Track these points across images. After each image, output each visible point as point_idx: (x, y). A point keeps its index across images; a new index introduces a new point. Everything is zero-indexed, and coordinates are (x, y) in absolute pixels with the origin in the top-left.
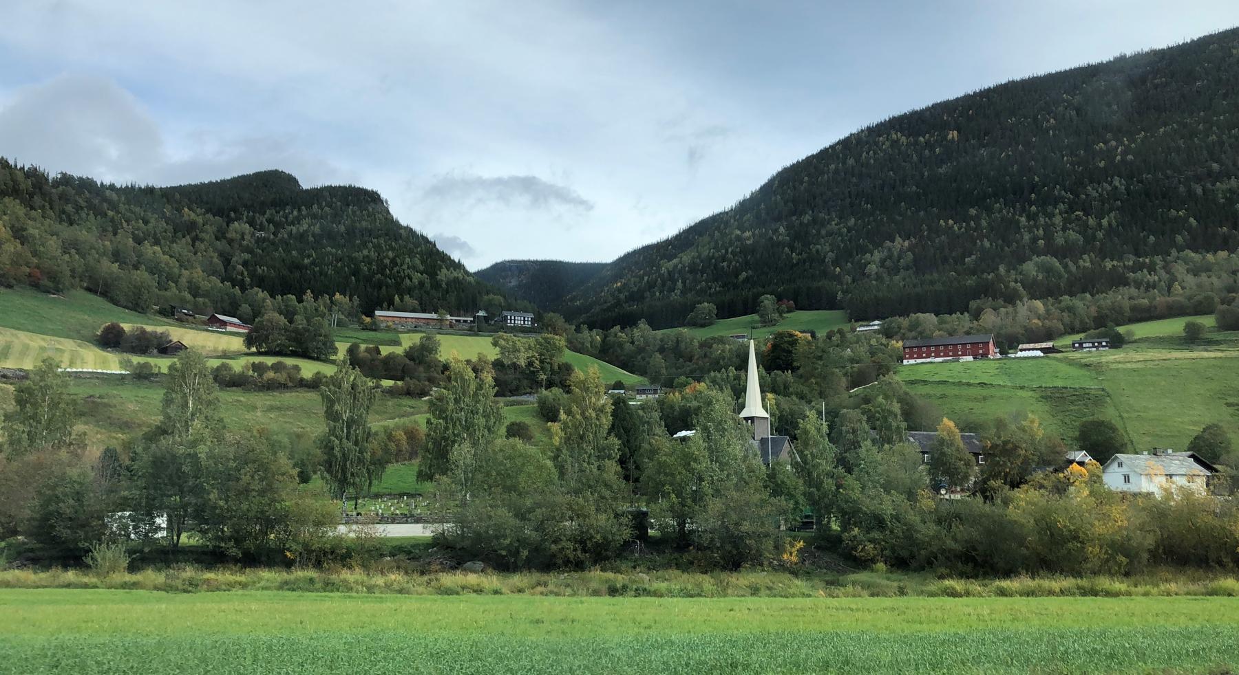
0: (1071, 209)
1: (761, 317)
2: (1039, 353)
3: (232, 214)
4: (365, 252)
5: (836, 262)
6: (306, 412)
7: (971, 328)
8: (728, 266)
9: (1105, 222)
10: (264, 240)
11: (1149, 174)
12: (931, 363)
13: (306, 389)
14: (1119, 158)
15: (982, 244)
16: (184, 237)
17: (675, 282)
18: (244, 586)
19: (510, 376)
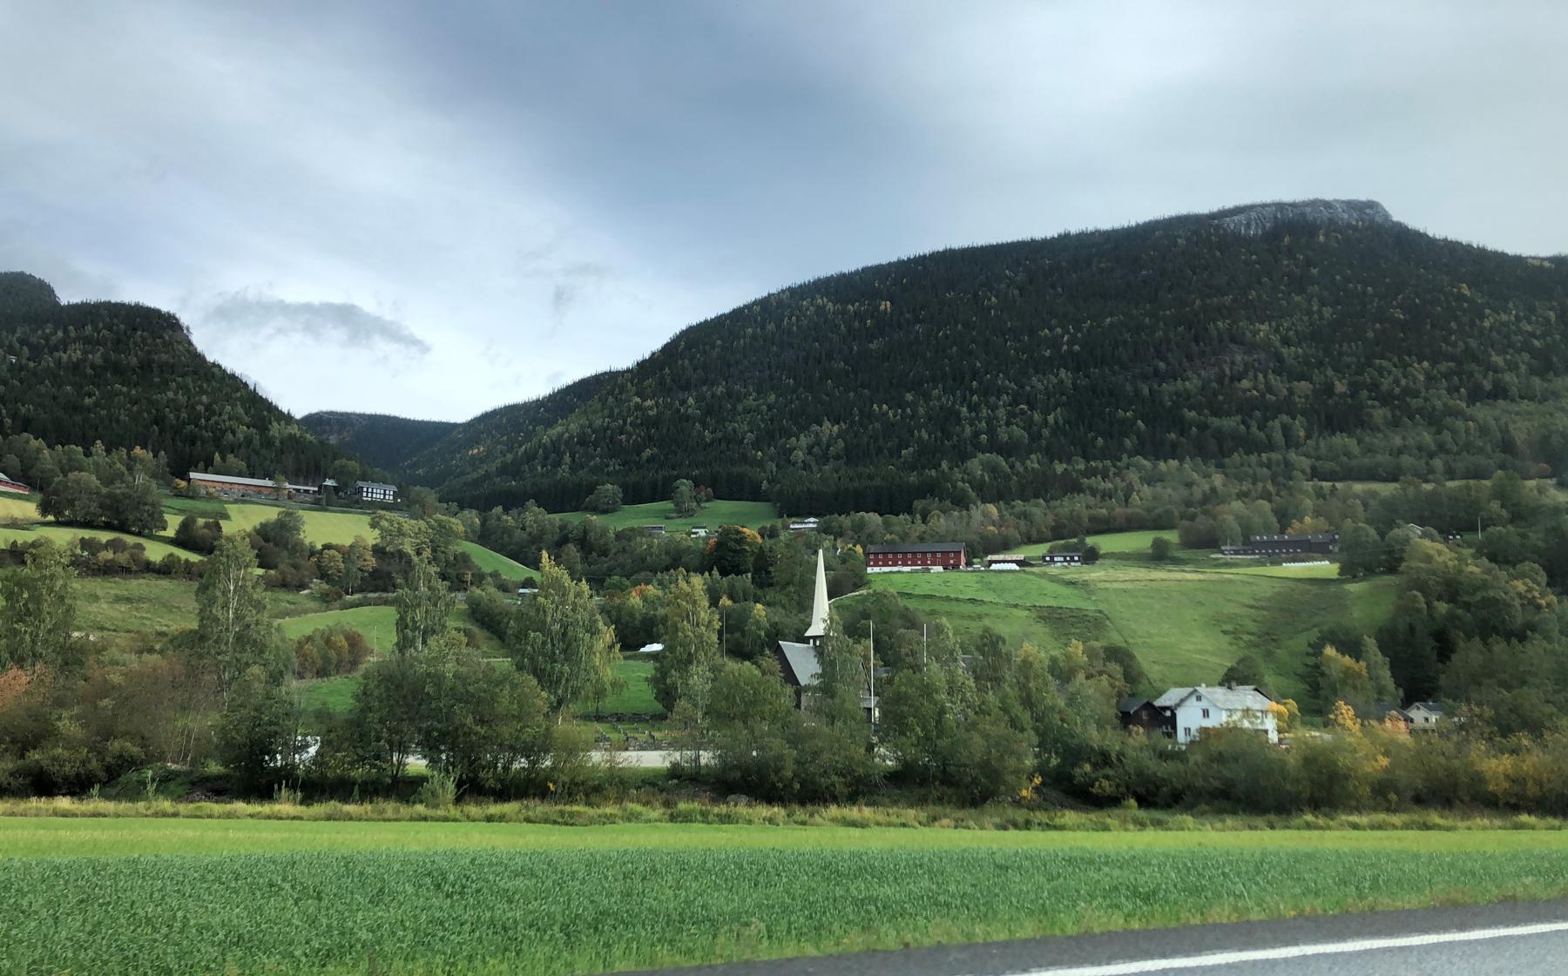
0: (1015, 403)
2: (1014, 567)
4: (170, 394)
5: (757, 445)
6: (164, 605)
7: (924, 532)
9: (1051, 418)
11: (1095, 368)
12: (899, 572)
13: (155, 575)
14: (1065, 347)
17: (560, 455)
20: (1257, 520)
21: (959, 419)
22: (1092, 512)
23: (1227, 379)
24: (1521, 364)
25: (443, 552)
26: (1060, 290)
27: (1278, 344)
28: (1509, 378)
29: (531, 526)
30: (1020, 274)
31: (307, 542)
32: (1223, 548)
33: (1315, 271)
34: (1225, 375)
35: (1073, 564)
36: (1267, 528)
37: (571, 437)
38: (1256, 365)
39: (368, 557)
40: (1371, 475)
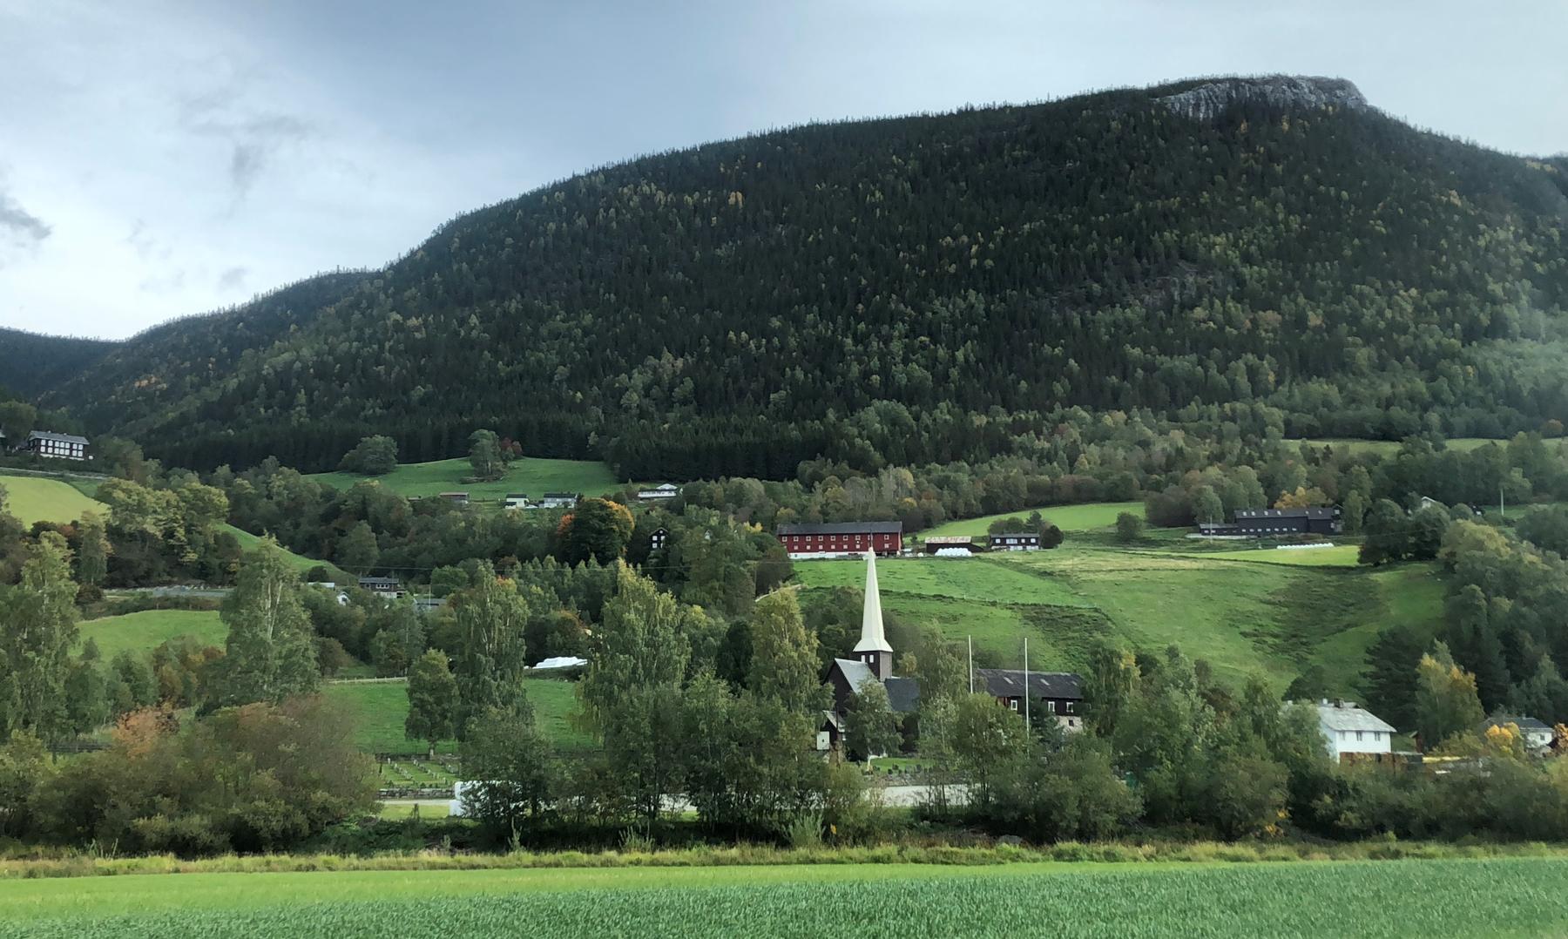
1: (473, 465)
2: (965, 552)
5: (573, 381)
8: (388, 373)
9: (960, 355)
14: (974, 262)
15: (793, 375)
17: (291, 394)
19: (134, 554)
20: (1242, 491)
21: (843, 355)
22: (1030, 478)
23: (1176, 306)
24: (1522, 294)
26: (963, 184)
27: (1237, 261)
28: (1509, 311)
30: (912, 162)
32: (1202, 526)
33: (1279, 168)
34: (1174, 302)
35: (1028, 548)
36: (1253, 501)
37: (305, 368)
38: (1212, 289)
40: (1359, 434)
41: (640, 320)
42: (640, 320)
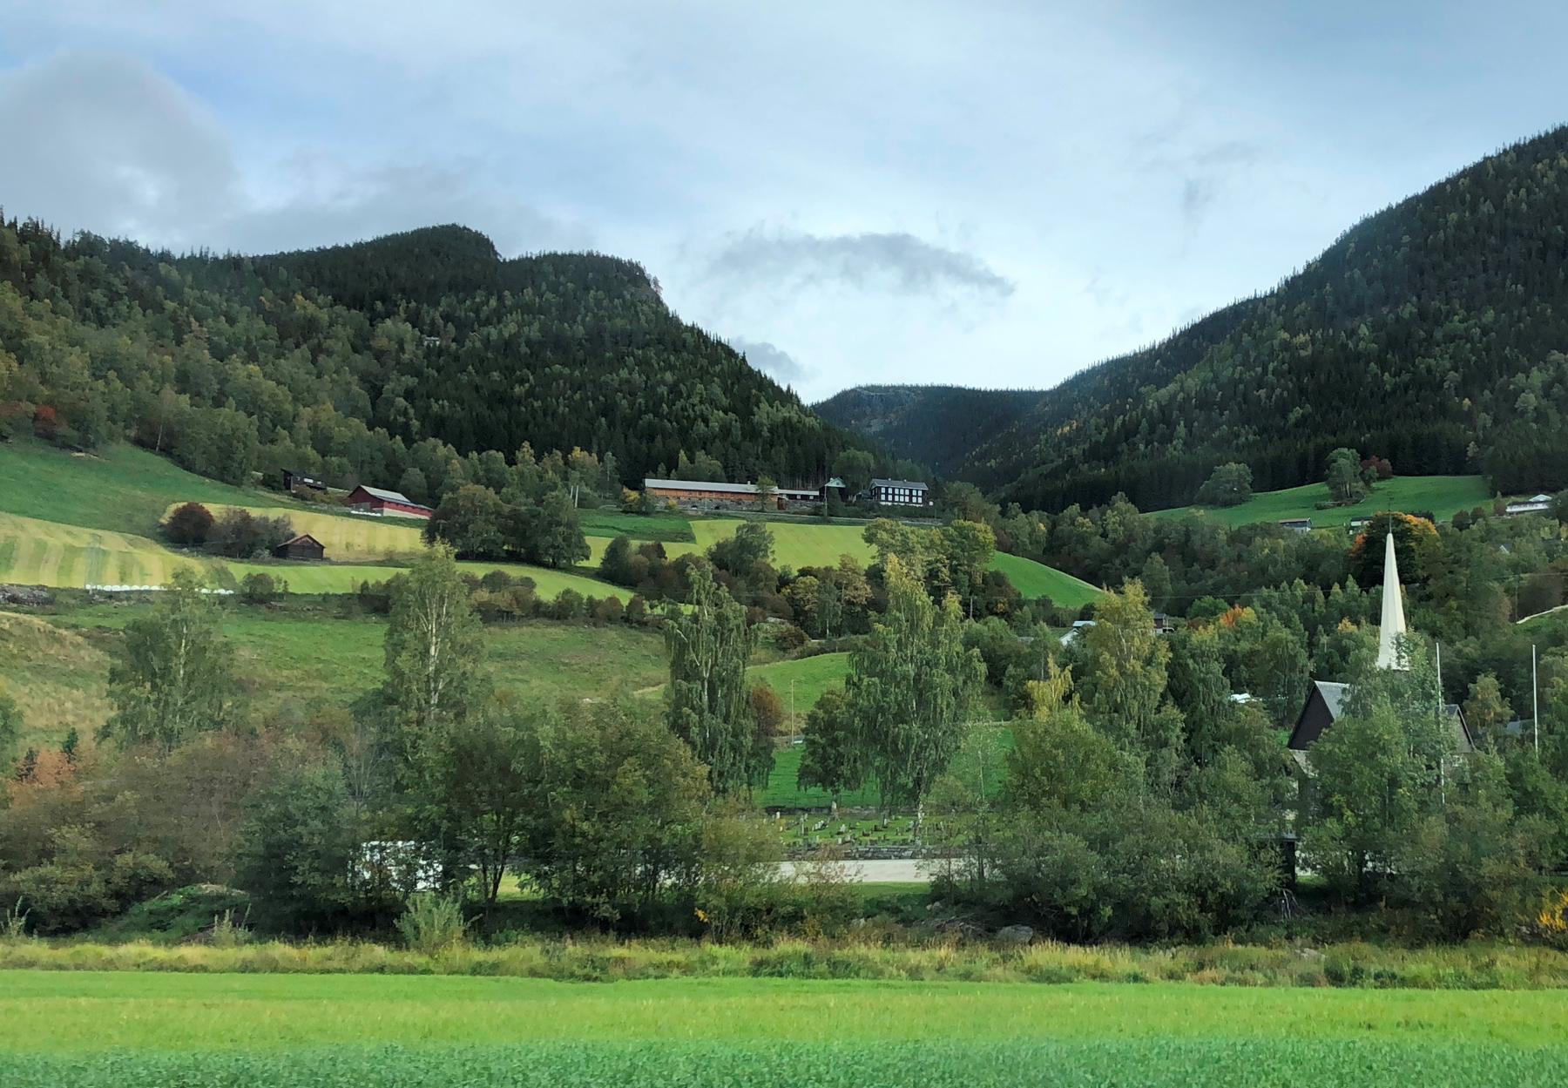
1: (1331, 488)
3: (379, 304)
4: (624, 373)
5: (1463, 389)
6: (551, 663)
8: (1269, 397)
10: (440, 352)
13: (546, 621)
16: (298, 346)
17: (1171, 425)
18: (687, 969)
25: (965, 573)
29: (1115, 531)
31: (777, 566)
37: (1187, 399)
39: (859, 585)
41: (1549, 311)
42: (1549, 311)
